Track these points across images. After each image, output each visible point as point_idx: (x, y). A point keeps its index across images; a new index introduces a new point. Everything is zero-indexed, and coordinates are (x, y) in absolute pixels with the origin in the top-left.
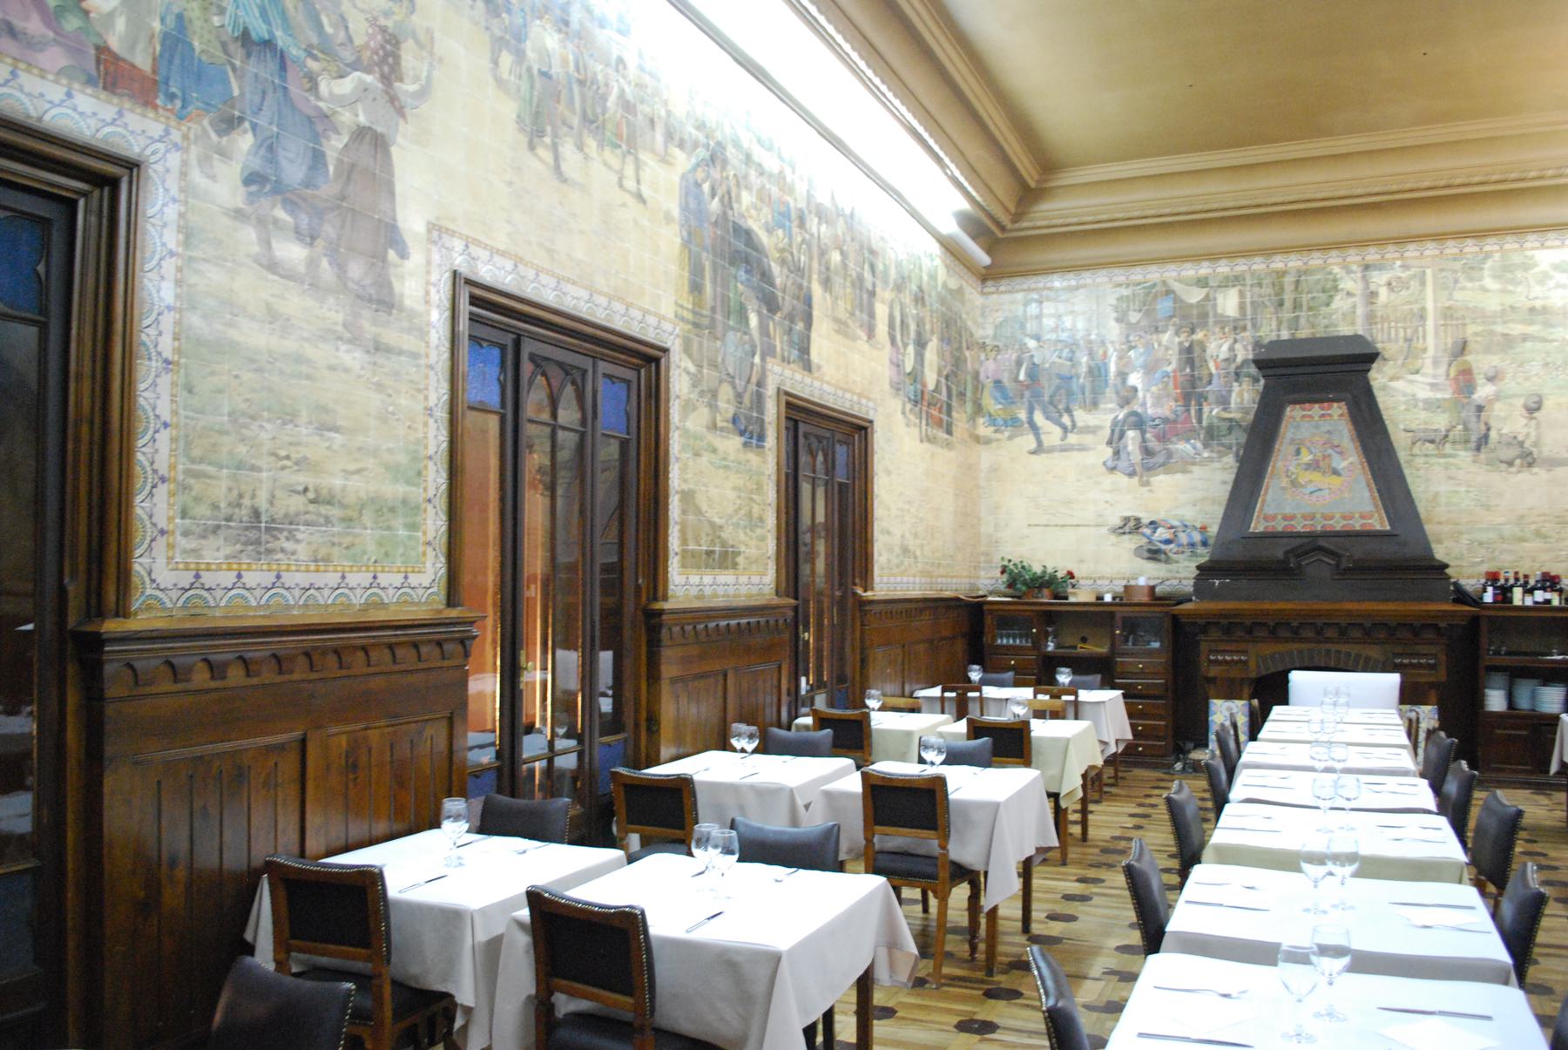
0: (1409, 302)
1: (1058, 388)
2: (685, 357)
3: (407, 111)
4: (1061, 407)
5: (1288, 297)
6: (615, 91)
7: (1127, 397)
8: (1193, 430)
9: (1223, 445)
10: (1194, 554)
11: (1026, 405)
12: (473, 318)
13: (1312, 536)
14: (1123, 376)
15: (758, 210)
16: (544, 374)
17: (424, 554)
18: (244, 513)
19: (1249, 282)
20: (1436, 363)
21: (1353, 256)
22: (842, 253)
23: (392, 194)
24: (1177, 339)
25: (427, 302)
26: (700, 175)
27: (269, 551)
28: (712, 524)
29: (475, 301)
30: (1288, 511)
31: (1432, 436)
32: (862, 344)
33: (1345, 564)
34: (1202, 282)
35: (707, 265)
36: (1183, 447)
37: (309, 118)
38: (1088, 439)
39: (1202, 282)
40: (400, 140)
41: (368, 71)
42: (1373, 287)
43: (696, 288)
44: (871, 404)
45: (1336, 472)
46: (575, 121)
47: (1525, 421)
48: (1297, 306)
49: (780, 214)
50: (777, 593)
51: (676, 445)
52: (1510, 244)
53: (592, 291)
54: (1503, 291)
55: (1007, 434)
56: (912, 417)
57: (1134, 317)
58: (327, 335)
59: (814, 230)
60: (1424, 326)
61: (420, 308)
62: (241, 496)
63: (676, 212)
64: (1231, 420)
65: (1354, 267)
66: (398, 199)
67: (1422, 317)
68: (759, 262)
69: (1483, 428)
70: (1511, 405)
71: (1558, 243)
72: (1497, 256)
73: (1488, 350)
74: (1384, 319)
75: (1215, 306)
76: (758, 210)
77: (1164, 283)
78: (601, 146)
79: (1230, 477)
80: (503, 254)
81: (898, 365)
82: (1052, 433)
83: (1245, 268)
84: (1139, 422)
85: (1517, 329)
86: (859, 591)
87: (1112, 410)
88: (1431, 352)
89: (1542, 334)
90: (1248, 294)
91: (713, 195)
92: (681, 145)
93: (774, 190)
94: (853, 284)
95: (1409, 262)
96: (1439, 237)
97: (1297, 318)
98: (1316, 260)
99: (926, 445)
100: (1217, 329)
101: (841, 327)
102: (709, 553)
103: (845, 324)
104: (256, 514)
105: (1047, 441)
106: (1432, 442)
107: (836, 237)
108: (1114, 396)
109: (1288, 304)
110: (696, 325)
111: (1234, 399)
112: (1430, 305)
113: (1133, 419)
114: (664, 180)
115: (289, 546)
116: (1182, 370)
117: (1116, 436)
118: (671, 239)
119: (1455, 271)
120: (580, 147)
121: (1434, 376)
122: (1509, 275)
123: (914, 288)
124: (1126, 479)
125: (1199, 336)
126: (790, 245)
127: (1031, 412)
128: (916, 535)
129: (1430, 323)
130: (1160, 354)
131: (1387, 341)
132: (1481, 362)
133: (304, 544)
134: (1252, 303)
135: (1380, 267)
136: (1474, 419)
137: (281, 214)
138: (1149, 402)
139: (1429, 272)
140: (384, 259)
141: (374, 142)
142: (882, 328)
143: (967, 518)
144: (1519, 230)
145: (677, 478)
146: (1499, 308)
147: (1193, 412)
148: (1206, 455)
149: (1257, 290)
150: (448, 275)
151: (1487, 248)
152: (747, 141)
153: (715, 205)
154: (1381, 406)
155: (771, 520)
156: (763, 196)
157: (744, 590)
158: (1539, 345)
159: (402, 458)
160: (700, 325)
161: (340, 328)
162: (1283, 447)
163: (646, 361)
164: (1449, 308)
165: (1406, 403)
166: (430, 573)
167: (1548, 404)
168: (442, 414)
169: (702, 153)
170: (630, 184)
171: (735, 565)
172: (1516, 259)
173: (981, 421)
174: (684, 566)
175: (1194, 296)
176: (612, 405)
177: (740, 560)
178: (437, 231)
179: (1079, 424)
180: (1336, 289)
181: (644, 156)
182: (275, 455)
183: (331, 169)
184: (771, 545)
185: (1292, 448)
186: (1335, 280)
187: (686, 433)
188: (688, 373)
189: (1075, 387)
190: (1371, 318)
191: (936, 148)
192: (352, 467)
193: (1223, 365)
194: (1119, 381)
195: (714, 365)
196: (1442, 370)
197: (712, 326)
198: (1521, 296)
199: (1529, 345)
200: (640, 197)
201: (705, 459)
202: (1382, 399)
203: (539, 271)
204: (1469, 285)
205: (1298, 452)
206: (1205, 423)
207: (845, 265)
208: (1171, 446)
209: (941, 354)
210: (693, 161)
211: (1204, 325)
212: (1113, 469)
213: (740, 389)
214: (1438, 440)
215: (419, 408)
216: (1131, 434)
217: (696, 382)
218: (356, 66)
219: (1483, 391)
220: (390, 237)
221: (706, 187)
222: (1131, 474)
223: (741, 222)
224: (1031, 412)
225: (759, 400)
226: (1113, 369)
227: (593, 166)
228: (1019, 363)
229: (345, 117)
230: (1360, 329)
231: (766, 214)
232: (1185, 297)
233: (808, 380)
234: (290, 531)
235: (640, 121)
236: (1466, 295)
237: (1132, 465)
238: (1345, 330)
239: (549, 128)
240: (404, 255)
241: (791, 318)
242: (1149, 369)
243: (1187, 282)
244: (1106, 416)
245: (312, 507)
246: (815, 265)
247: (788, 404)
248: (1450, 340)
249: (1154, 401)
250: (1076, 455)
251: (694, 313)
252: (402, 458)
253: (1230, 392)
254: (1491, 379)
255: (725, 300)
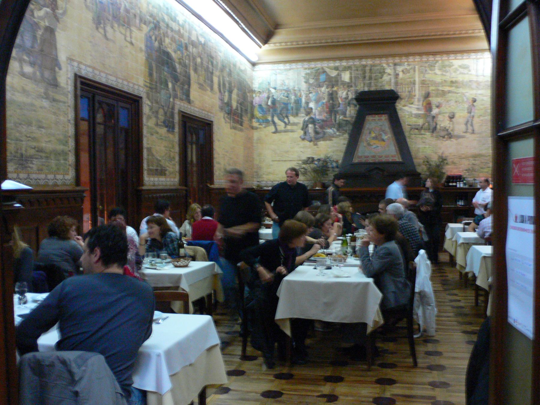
0: (410, 78)
1: (283, 109)
3: (60, 20)
4: (284, 115)
5: (367, 75)
6: (123, 6)
7: (309, 111)
9: (343, 130)
10: (334, 171)
11: (271, 115)
12: (82, 89)
13: (374, 163)
14: (307, 103)
15: (171, 44)
16: (102, 108)
17: (68, 169)
18: (19, 155)
20: (419, 100)
21: (391, 60)
22: (201, 58)
23: (56, 49)
24: (327, 90)
25: (67, 84)
26: (151, 33)
27: (26, 167)
28: (157, 159)
29: (82, 83)
30: (366, 154)
31: (417, 127)
32: (209, 93)
34: (336, 68)
35: (154, 66)
36: (330, 131)
37: (32, 25)
38: (295, 128)
39: (336, 68)
40: (58, 30)
41: (48, 7)
42: (397, 72)
43: (151, 75)
44: (212, 115)
46: (110, 18)
47: (448, 122)
48: (370, 78)
49: (178, 45)
50: (180, 185)
51: (145, 131)
52: (445, 57)
53: (117, 78)
54: (442, 75)
55: (264, 126)
56: (227, 119)
57: (311, 81)
58: (40, 97)
60: (415, 87)
61: (65, 86)
62: (18, 149)
63: (143, 47)
64: (347, 121)
65: (391, 64)
66: (58, 50)
67: (414, 83)
68: (172, 64)
69: (434, 124)
70: (444, 116)
71: (460, 58)
72: (440, 62)
73: (437, 96)
74: (402, 84)
75: (341, 77)
76: (171, 44)
77: (322, 68)
78: (119, 25)
79: (346, 142)
80: (89, 66)
81: (222, 100)
82: (281, 125)
83: (352, 63)
84: (313, 121)
85: (447, 89)
86: (209, 185)
87: (303, 117)
88: (417, 96)
89: (455, 91)
91: (156, 40)
92: (145, 24)
93: (177, 37)
94: (205, 70)
95: (410, 63)
96: (420, 54)
97: (370, 83)
98: (377, 61)
99: (233, 130)
100: (342, 86)
101: (201, 87)
102: (157, 170)
103: (202, 85)
104: (22, 155)
106: (417, 129)
108: (304, 111)
109: (367, 78)
112: (417, 79)
113: (311, 120)
114: (139, 36)
115: (31, 165)
117: (305, 126)
118: (142, 57)
120: (112, 27)
121: (418, 105)
122: (444, 69)
123: (228, 70)
124: (308, 142)
126: (182, 57)
127: (273, 117)
128: (229, 165)
129: (417, 86)
130: (321, 95)
131: (402, 91)
132: (434, 100)
133: (35, 165)
134: (355, 77)
135: (400, 64)
136: (431, 121)
137: (25, 57)
138: (317, 114)
139: (417, 67)
140: (55, 71)
141: (50, 31)
142: (216, 86)
144: (448, 53)
145: (146, 143)
146: (440, 81)
147: (333, 118)
148: (338, 134)
149: (356, 72)
150: (73, 75)
151: (437, 59)
152: (166, 18)
153: (156, 44)
154: (400, 116)
155: (177, 158)
156: (173, 39)
157: (168, 183)
159: (61, 137)
161: (43, 95)
162: (365, 131)
163: (134, 102)
164: (423, 80)
165: (408, 115)
166: (71, 175)
167: (457, 116)
168: (73, 122)
169: (152, 25)
170: (128, 39)
171: (165, 174)
172: (447, 63)
173: (254, 120)
174: (148, 174)
175: (334, 74)
176: (123, 119)
177: (167, 172)
178: (70, 59)
179: (291, 122)
180: (384, 72)
181: (133, 28)
182: (27, 136)
183: (39, 41)
184: (177, 168)
185: (368, 131)
186: (384, 69)
188: (148, 105)
189: (289, 108)
190: (396, 83)
191: (236, 18)
192: (47, 140)
193: (344, 100)
194: (306, 106)
195: (157, 102)
196: (421, 103)
197: (156, 89)
198: (448, 77)
200: (132, 43)
201: (154, 137)
202: (400, 114)
203: (100, 71)
204: (431, 72)
205: (370, 133)
206: (337, 122)
207: (202, 63)
208: (325, 131)
209: (238, 95)
210: (149, 28)
211: (337, 85)
212: (303, 139)
213: (166, 111)
214: (419, 129)
215: (66, 120)
216: (310, 126)
217: (151, 109)
218: (44, 6)
219: (435, 111)
220: (55, 63)
221: (153, 38)
222: (310, 141)
223: (165, 49)
224: (273, 117)
225: (172, 115)
226: (303, 100)
227: (116, 33)
229: (42, 24)
231: (174, 46)
232: (329, 74)
233: (189, 107)
234: (31, 161)
235: (131, 16)
236: (429, 76)
237: (311, 137)
238: (387, 88)
239: (102, 21)
240: (60, 69)
241: (183, 84)
242: (317, 101)
244: (301, 119)
245: (37, 153)
247: (183, 116)
248: (423, 92)
250: (290, 134)
251: (150, 84)
253: (346, 110)
255: (160, 78)
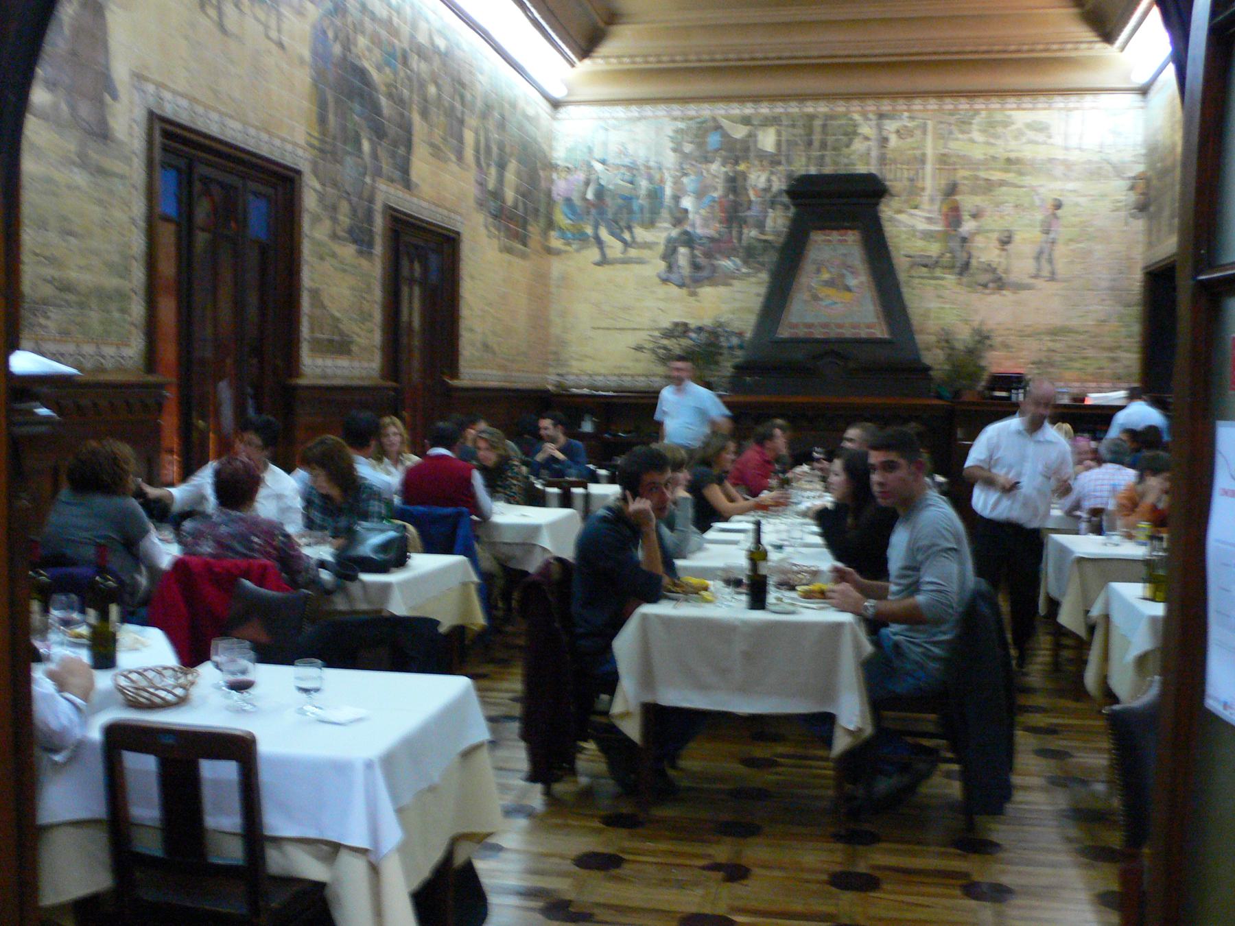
0: (914, 149)
1: (620, 208)
2: (313, 177)
4: (622, 224)
5: (817, 138)
7: (680, 217)
8: (734, 249)
9: (758, 263)
12: (165, 149)
13: (826, 342)
14: (676, 199)
19: (785, 123)
20: (932, 200)
21: (871, 106)
24: (724, 169)
26: (326, 23)
28: (333, 316)
30: (809, 320)
31: (925, 261)
32: (454, 167)
33: (851, 365)
34: (746, 121)
36: (726, 264)
38: (646, 253)
39: (746, 121)
42: (885, 133)
43: (322, 120)
45: (848, 289)
47: (997, 252)
48: (824, 145)
51: (307, 250)
52: (995, 104)
57: (688, 148)
59: (415, 66)
63: (306, 53)
64: (765, 241)
65: (871, 116)
67: (922, 160)
68: (371, 96)
70: (988, 238)
72: (984, 113)
74: (894, 161)
75: (756, 142)
76: (370, 50)
77: (714, 119)
79: (763, 290)
81: (482, 184)
82: (614, 247)
83: (782, 110)
84: (689, 240)
85: (996, 176)
88: (928, 192)
90: (784, 133)
93: (383, 33)
96: (940, 94)
98: (840, 107)
99: (506, 256)
100: (756, 162)
103: (438, 148)
105: (611, 254)
106: (925, 266)
107: (433, 72)
109: (816, 144)
110: (322, 151)
111: (769, 223)
112: (929, 152)
115: (42, 321)
116: (726, 196)
118: (303, 78)
119: (950, 124)
122: (992, 131)
123: (496, 115)
125: (742, 167)
127: (596, 227)
129: (929, 168)
131: (895, 178)
132: (968, 202)
139: (930, 124)
142: (469, 153)
143: (540, 320)
144: (1002, 93)
145: (308, 278)
148: (744, 270)
149: (790, 130)
151: (977, 106)
153: (337, 49)
154: (887, 235)
155: (378, 316)
156: (376, 40)
157: (356, 373)
158: (1013, 190)
159: (116, 258)
160: (326, 151)
163: (281, 182)
166: (134, 349)
167: (1018, 238)
172: (998, 116)
173: (552, 233)
174: (312, 350)
175: (739, 132)
177: (354, 348)
178: (139, 77)
179: (639, 239)
180: (855, 133)
184: (377, 337)
187: (312, 239)
189: (635, 207)
190: (883, 160)
195: (335, 184)
196: (936, 207)
197: (334, 153)
199: (1004, 189)
200: (281, 45)
202: (889, 230)
204: (960, 136)
207: (439, 97)
208: (716, 262)
209: (518, 174)
211: (746, 159)
212: (665, 281)
214: (930, 265)
217: (322, 197)
219: (968, 226)
220: (104, 85)
221: (331, 34)
222: (681, 286)
223: (357, 62)
224: (596, 227)
228: (587, 183)
230: (873, 169)
233: (407, 196)
236: (958, 145)
237: (682, 277)
238: (861, 169)
240: (115, 97)
241: (395, 144)
242: (700, 194)
243: (733, 120)
244: (662, 233)
246: (415, 97)
249: (701, 221)
250: (637, 268)
252: (116, 258)
253: (765, 217)
254: (975, 216)
255: (344, 129)
